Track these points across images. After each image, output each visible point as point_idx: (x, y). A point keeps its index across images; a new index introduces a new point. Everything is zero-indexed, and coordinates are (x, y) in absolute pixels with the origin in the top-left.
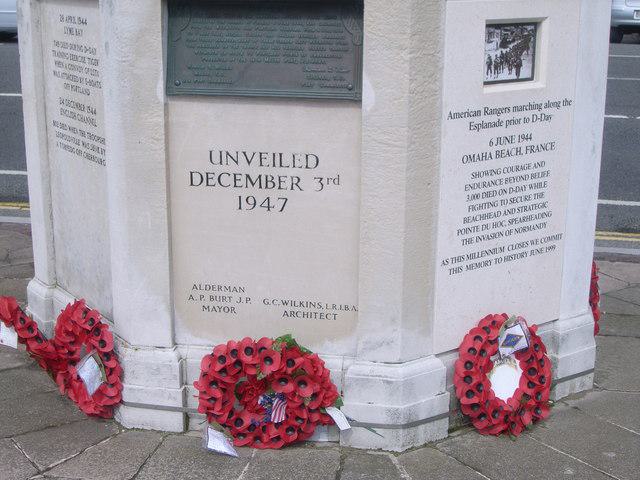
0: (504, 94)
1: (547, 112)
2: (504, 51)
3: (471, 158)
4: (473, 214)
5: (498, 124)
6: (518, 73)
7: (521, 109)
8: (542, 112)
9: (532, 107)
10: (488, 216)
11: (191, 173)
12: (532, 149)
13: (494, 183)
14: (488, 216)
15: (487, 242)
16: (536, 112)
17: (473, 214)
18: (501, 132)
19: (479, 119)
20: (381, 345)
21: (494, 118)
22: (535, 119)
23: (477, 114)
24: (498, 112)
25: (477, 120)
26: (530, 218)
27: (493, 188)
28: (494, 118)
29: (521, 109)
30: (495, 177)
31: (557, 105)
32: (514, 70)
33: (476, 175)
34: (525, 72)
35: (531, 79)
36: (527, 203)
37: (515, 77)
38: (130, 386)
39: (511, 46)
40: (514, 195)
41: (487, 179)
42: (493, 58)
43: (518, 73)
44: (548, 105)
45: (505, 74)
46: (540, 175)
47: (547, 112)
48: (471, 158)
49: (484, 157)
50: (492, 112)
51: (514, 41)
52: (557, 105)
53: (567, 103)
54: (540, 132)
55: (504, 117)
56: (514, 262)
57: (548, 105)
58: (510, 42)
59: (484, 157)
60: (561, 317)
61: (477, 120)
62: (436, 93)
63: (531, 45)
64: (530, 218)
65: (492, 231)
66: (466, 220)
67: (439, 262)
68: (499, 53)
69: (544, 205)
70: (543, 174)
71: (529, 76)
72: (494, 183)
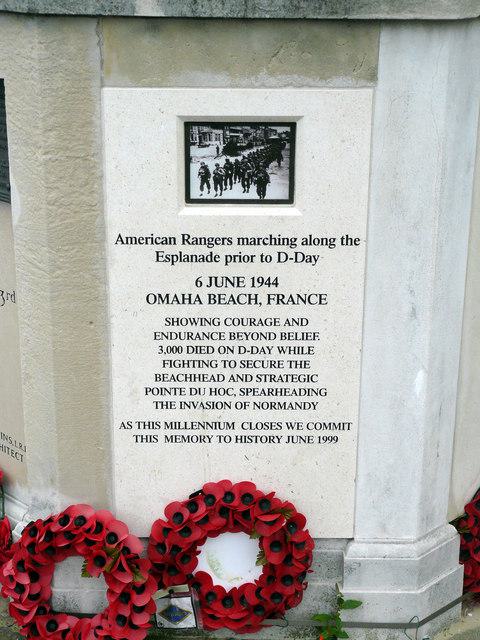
0: (237, 219)
1: (309, 250)
2: (232, 160)
3: (162, 299)
4: (170, 371)
5: (213, 258)
6: (262, 191)
7: (256, 242)
8: (296, 250)
9: (273, 240)
10: (202, 378)
11: (158, 253)
12: (280, 299)
13: (210, 336)
14: (202, 378)
15: (199, 410)
16: (284, 248)
17: (170, 371)
18: (219, 269)
19: (168, 249)
20: (45, 508)
21: (203, 250)
22: (281, 258)
23: (170, 241)
24: (210, 242)
25: (169, 250)
26: (284, 392)
27: (206, 342)
28: (203, 250)
29: (256, 242)
30: (208, 329)
31: (330, 243)
32: (253, 188)
33: (171, 322)
34: (276, 189)
35: (290, 201)
36: (276, 372)
37: (256, 197)
38: (320, 551)
39: (246, 153)
40: (247, 357)
41: (195, 329)
42: (212, 169)
43: (262, 191)
44: (307, 242)
45: (236, 191)
46: (302, 341)
47: (309, 250)
48: (162, 299)
49: (186, 299)
50: (197, 241)
51: (250, 146)
52: (330, 243)
53: (348, 241)
54: (294, 278)
55: (221, 250)
56: (252, 447)
57: (307, 242)
58: (243, 149)
59: (186, 299)
60: (357, 538)
61: (169, 250)
62: (96, 207)
63: (285, 153)
64: (284, 392)
65: (207, 398)
66: (158, 378)
67: (117, 424)
68: (222, 162)
69: (310, 379)
70: (305, 336)
71: (286, 197)
72: (210, 336)
